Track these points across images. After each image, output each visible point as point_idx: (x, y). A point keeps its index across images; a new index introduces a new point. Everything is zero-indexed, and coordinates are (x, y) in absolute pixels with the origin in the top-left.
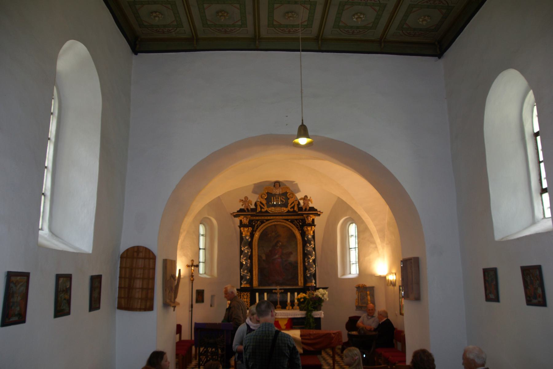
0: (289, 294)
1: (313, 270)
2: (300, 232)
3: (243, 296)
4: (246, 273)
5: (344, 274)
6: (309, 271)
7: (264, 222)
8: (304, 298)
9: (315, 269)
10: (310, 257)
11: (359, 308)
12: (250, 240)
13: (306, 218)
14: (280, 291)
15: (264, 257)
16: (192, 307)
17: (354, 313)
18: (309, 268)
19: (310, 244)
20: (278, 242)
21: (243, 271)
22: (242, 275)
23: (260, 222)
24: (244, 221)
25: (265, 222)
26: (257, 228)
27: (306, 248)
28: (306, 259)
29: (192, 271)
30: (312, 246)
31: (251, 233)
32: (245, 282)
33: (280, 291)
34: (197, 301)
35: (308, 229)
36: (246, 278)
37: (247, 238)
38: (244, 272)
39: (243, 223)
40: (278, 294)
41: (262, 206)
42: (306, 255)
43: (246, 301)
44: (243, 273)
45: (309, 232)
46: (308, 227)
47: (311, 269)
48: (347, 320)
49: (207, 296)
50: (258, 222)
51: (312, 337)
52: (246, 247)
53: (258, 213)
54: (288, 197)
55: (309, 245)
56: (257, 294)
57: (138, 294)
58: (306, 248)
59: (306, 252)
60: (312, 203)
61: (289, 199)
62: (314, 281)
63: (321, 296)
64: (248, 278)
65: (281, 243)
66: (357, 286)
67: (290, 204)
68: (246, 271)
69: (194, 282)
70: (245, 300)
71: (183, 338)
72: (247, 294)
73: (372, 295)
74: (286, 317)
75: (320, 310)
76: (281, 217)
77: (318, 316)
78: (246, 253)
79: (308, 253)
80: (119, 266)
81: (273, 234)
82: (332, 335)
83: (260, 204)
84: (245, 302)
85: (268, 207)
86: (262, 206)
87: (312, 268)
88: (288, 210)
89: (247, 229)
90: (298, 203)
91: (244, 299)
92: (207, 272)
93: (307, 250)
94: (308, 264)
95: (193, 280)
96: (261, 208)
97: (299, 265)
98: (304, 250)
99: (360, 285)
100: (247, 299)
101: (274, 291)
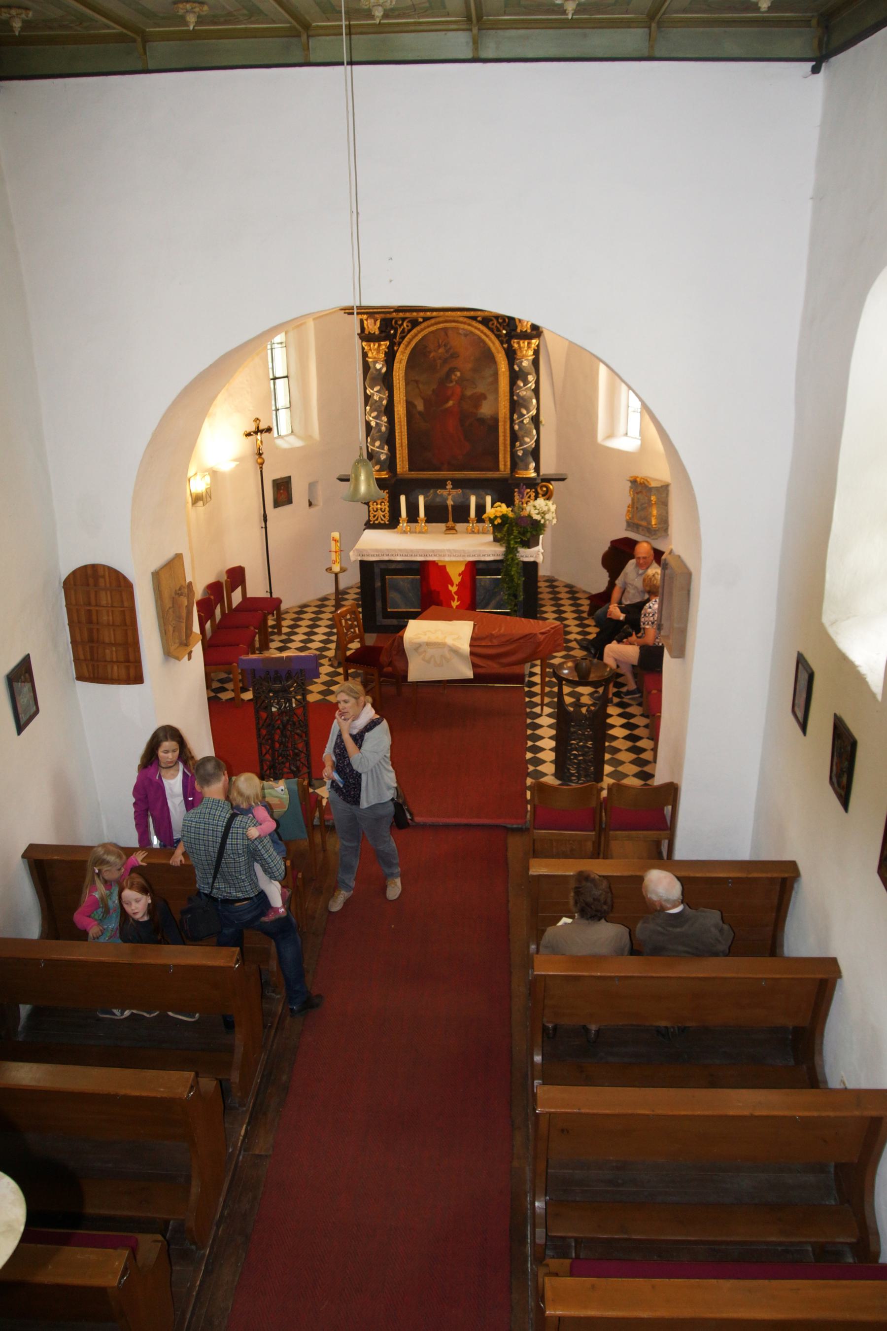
1: (530, 442)
2: (288, 863)
5: (611, 435)
6: (521, 445)
8: (504, 517)
9: (535, 437)
10: (524, 412)
11: (631, 525)
12: (384, 370)
15: (420, 406)
16: (265, 520)
17: (621, 532)
18: (523, 437)
19: (526, 382)
20: (452, 370)
21: (373, 441)
22: (370, 449)
23: (408, 322)
24: (368, 327)
25: (421, 323)
26: (403, 338)
27: (518, 391)
28: (515, 416)
29: (259, 442)
30: (531, 387)
31: (386, 354)
34: (277, 504)
35: (522, 345)
36: (380, 459)
38: (374, 446)
39: (367, 332)
42: (515, 405)
43: (381, 509)
44: (372, 447)
45: (525, 352)
46: (521, 342)
47: (527, 439)
48: (606, 547)
49: (298, 490)
50: (405, 325)
51: (495, 642)
52: (375, 389)
55: (522, 384)
57: (110, 653)
58: (518, 391)
59: (515, 398)
63: (537, 517)
64: (383, 457)
65: (458, 374)
66: (631, 479)
68: (377, 443)
69: (264, 466)
70: (379, 506)
71: (249, 595)
73: (664, 504)
74: (461, 559)
76: (459, 313)
77: (532, 559)
78: (376, 401)
79: (521, 401)
80: (64, 603)
81: (441, 350)
82: (540, 636)
84: (379, 511)
87: (527, 437)
89: (377, 345)
91: (377, 504)
92: (296, 430)
93: (518, 395)
94: (520, 428)
95: (262, 464)
97: (501, 424)
98: (512, 393)
99: (638, 477)
100: (375, 510)
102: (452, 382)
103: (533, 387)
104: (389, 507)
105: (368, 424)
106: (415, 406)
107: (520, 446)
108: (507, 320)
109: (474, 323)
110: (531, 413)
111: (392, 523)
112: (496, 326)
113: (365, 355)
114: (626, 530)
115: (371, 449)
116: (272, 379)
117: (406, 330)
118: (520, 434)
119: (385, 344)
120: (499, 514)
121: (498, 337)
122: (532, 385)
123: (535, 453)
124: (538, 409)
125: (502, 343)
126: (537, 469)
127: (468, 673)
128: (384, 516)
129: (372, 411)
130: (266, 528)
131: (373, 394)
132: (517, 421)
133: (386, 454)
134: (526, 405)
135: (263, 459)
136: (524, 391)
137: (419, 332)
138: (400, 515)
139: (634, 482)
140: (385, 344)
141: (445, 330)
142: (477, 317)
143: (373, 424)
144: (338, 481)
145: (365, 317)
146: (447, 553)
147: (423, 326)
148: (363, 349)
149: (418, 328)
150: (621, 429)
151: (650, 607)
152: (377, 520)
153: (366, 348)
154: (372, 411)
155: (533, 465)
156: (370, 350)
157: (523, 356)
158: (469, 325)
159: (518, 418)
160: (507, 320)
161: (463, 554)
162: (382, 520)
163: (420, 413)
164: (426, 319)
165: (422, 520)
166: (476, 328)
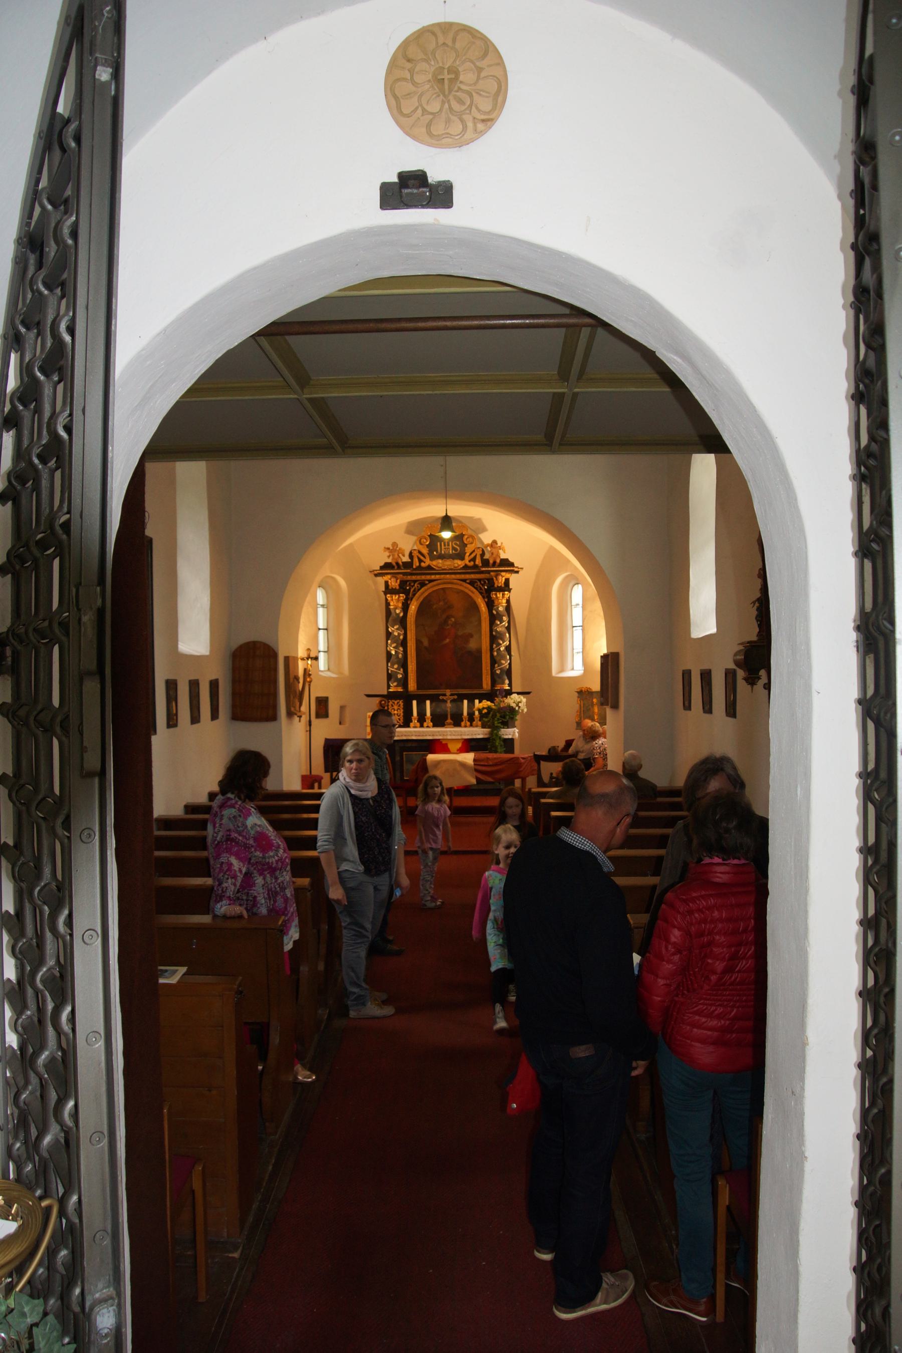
1: (505, 664)
5: (562, 670)
7: (426, 585)
8: (489, 708)
9: (509, 662)
10: (501, 642)
12: (402, 615)
13: (494, 578)
14: (452, 697)
15: (426, 643)
16: (310, 725)
18: (500, 660)
19: (502, 621)
20: (448, 617)
21: (392, 666)
22: (390, 672)
23: (419, 584)
25: (427, 584)
26: (414, 595)
28: (494, 646)
31: (403, 604)
32: (395, 684)
34: (318, 716)
35: (498, 595)
38: (393, 668)
39: (390, 588)
40: (449, 701)
41: (422, 558)
42: (494, 639)
47: (503, 662)
49: (333, 708)
50: (416, 585)
52: (395, 628)
53: (415, 569)
55: (499, 623)
56: (415, 703)
59: (494, 633)
60: (504, 552)
61: (466, 545)
64: (400, 676)
66: (578, 690)
67: (468, 554)
68: (396, 666)
70: (396, 712)
72: (398, 703)
74: (459, 737)
77: (510, 737)
79: (498, 635)
81: (441, 603)
82: (521, 759)
83: (418, 554)
84: (396, 709)
85: (431, 559)
86: (422, 558)
87: (504, 660)
88: (466, 565)
89: (397, 597)
90: (481, 552)
93: (496, 631)
96: (420, 561)
98: (491, 630)
101: (441, 697)
102: (448, 625)
103: (507, 625)
104: (403, 712)
105: (389, 654)
107: (498, 666)
109: (464, 584)
110: (505, 643)
113: (388, 604)
114: (577, 729)
115: (391, 671)
118: (497, 659)
122: (505, 624)
123: (509, 673)
125: (484, 597)
128: (399, 719)
130: (310, 731)
132: (495, 649)
135: (311, 678)
136: (501, 627)
137: (426, 591)
138: (412, 715)
142: (467, 580)
143: (393, 652)
144: (365, 697)
146: (449, 733)
147: (429, 586)
148: (386, 600)
149: (425, 588)
150: (569, 666)
153: (389, 599)
155: (507, 682)
156: (392, 600)
157: (499, 603)
158: (461, 585)
159: (496, 647)
161: (460, 734)
165: (428, 719)
166: (466, 588)
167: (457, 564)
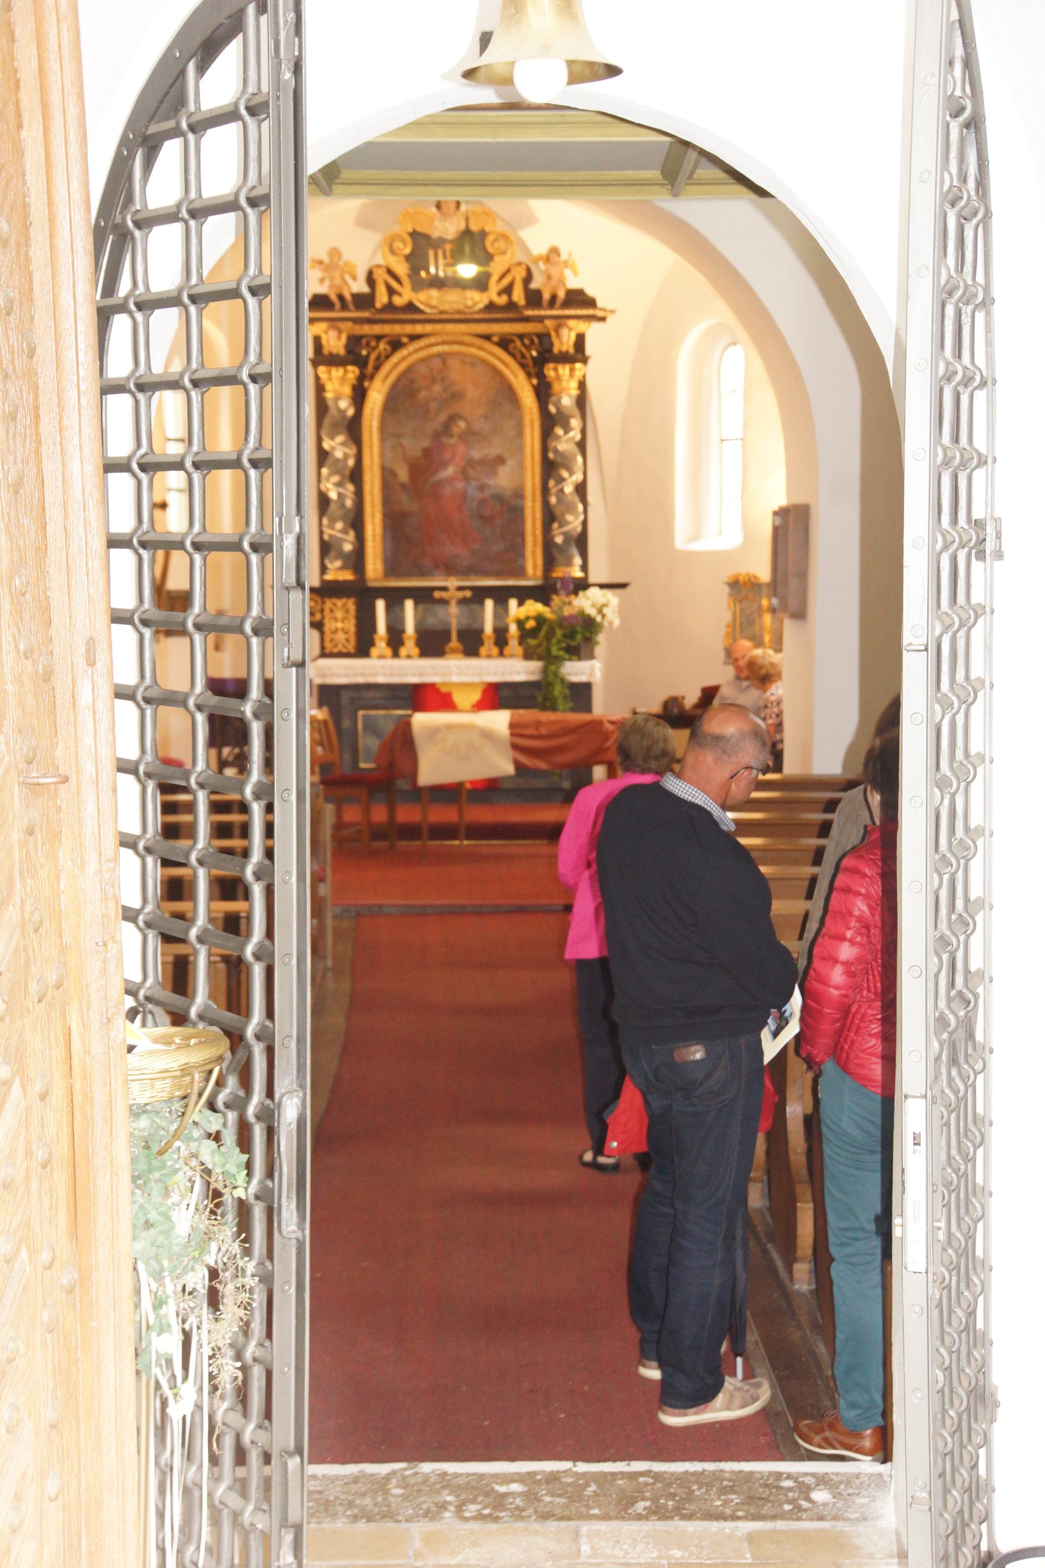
0: (489, 604)
1: (574, 523)
3: (332, 611)
4: (341, 531)
5: (696, 537)
6: (561, 526)
8: (540, 619)
15: (403, 474)
18: (563, 515)
19: (567, 429)
20: (452, 419)
21: (331, 526)
26: (377, 368)
28: (551, 483)
30: (574, 438)
33: (461, 594)
37: (343, 404)
38: (333, 528)
40: (453, 603)
42: (550, 467)
47: (570, 518)
54: (490, 250)
56: (380, 605)
59: (551, 455)
62: (578, 561)
66: (731, 580)
67: (495, 278)
74: (476, 679)
75: (591, 656)
81: (437, 388)
96: (391, 292)
98: (545, 449)
101: (437, 594)
102: (451, 436)
106: (394, 474)
108: (536, 340)
111: (363, 648)
112: (521, 352)
116: (122, 693)
117: (383, 356)
118: (558, 511)
119: (353, 371)
120: (532, 613)
121: (523, 366)
122: (575, 435)
123: (581, 542)
124: (585, 473)
125: (529, 375)
126: (584, 567)
127: (504, 766)
129: (331, 474)
131: (333, 448)
133: (352, 543)
134: (566, 463)
136: (565, 442)
139: (735, 584)
140: (353, 371)
141: (441, 356)
143: (333, 495)
145: (323, 326)
151: (772, 694)
152: (336, 646)
154: (331, 474)
160: (536, 340)
162: (344, 646)
163: (403, 486)
164: (414, 338)
167: (472, 299)
